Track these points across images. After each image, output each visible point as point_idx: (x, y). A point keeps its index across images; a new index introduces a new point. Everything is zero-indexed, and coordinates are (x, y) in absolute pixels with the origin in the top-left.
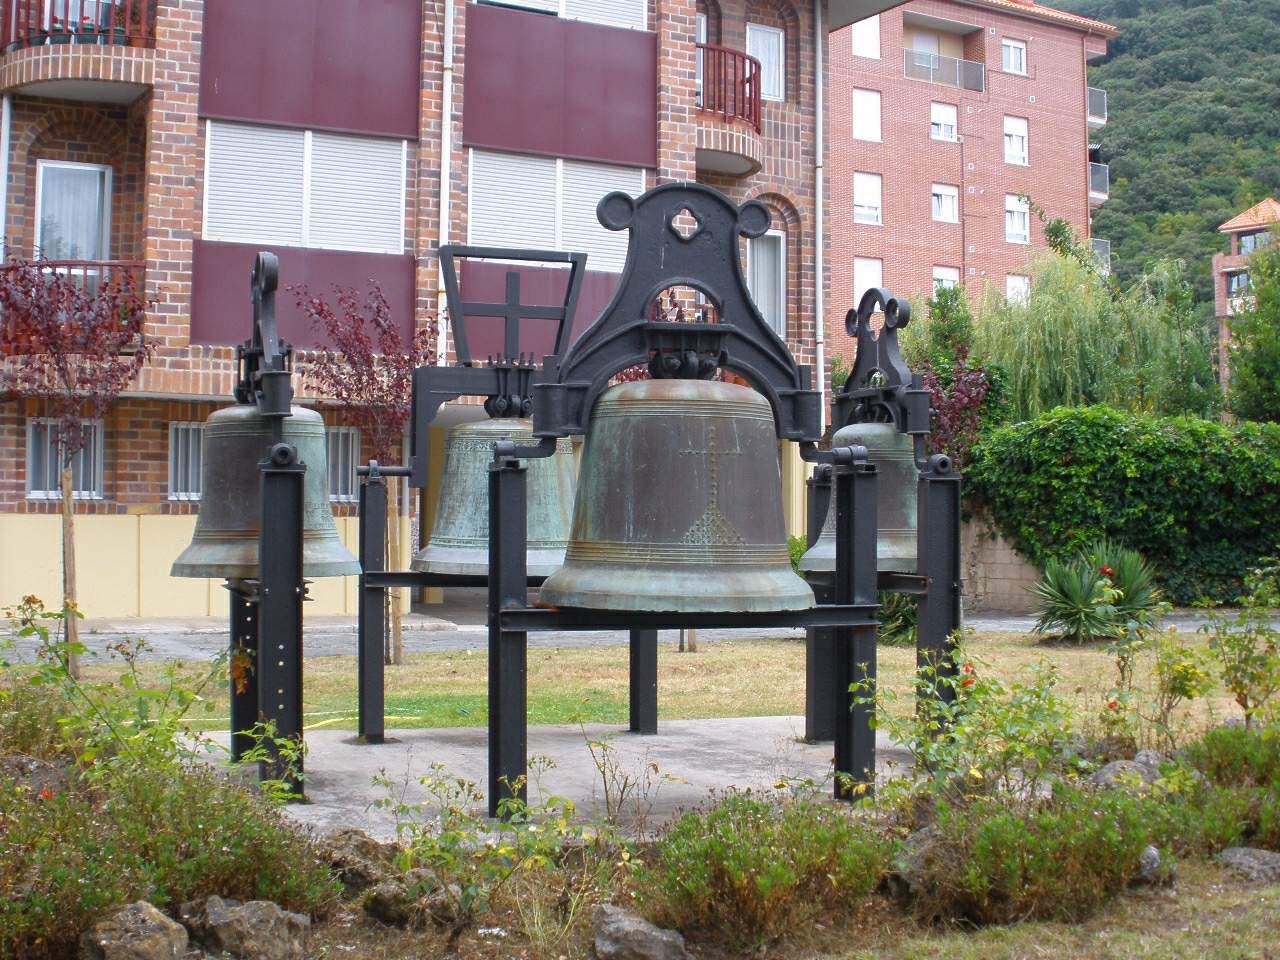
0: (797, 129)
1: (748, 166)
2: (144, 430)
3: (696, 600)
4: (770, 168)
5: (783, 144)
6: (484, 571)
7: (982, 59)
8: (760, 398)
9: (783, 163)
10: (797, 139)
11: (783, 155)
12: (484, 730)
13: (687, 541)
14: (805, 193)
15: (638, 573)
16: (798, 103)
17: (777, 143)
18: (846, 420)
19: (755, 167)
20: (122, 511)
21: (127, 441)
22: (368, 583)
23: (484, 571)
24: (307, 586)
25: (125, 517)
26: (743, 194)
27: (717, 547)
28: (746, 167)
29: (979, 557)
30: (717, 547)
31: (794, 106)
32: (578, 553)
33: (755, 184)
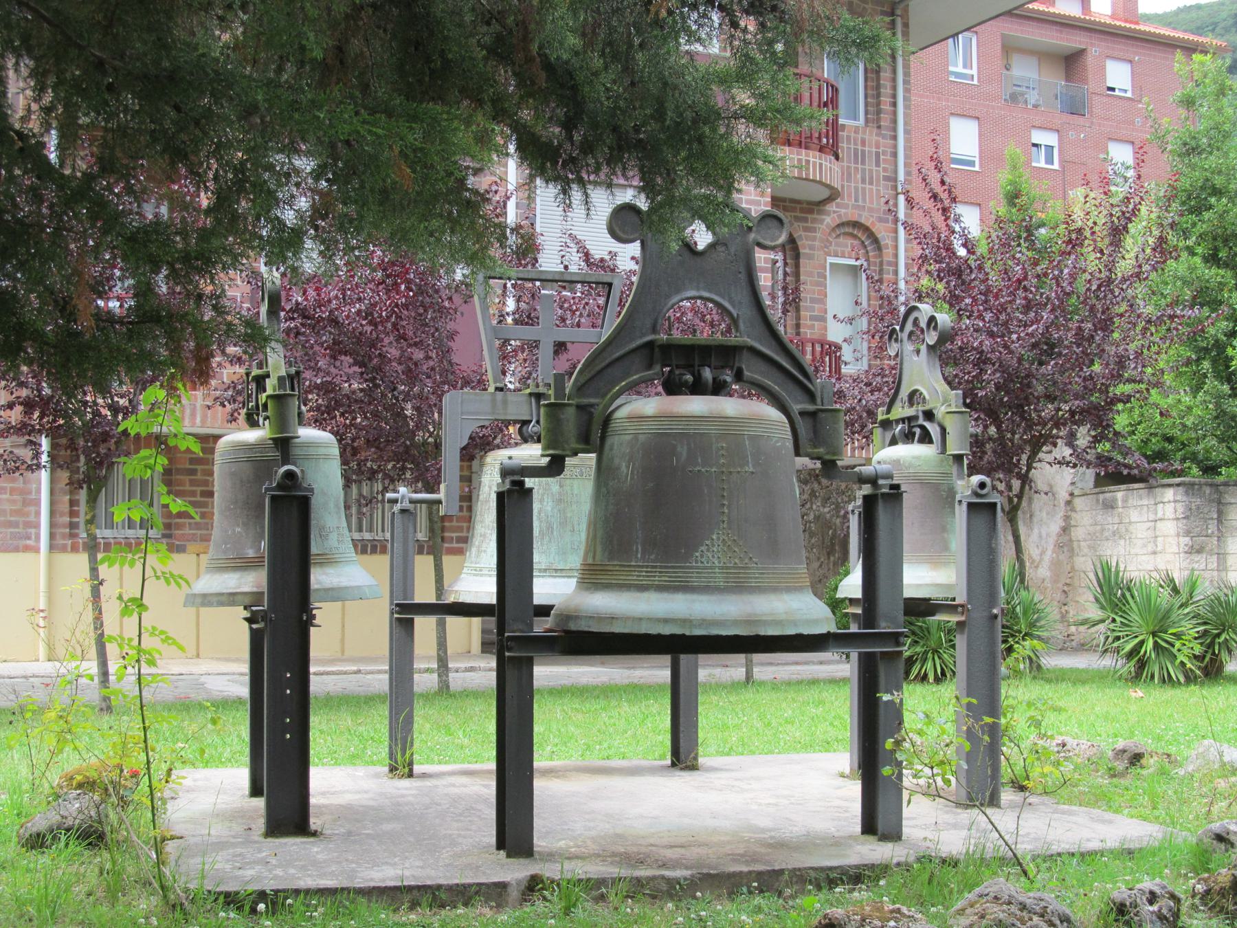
0: (878, 155)
1: (825, 193)
2: (202, 467)
3: (704, 622)
4: (849, 196)
5: (864, 170)
6: (492, 599)
7: (1085, 81)
8: (773, 413)
9: (864, 189)
10: (878, 165)
11: (863, 181)
12: (492, 766)
13: (696, 562)
14: (886, 221)
15: (646, 595)
16: (879, 127)
17: (856, 169)
18: (887, 442)
19: (834, 195)
20: (181, 549)
21: (186, 478)
22: (509, 650)
23: (492, 599)
24: (314, 612)
25: (182, 555)
26: (822, 221)
27: (727, 568)
28: (821, 194)
29: (1070, 596)
30: (727, 568)
31: (875, 130)
32: (593, 577)
33: (834, 212)
